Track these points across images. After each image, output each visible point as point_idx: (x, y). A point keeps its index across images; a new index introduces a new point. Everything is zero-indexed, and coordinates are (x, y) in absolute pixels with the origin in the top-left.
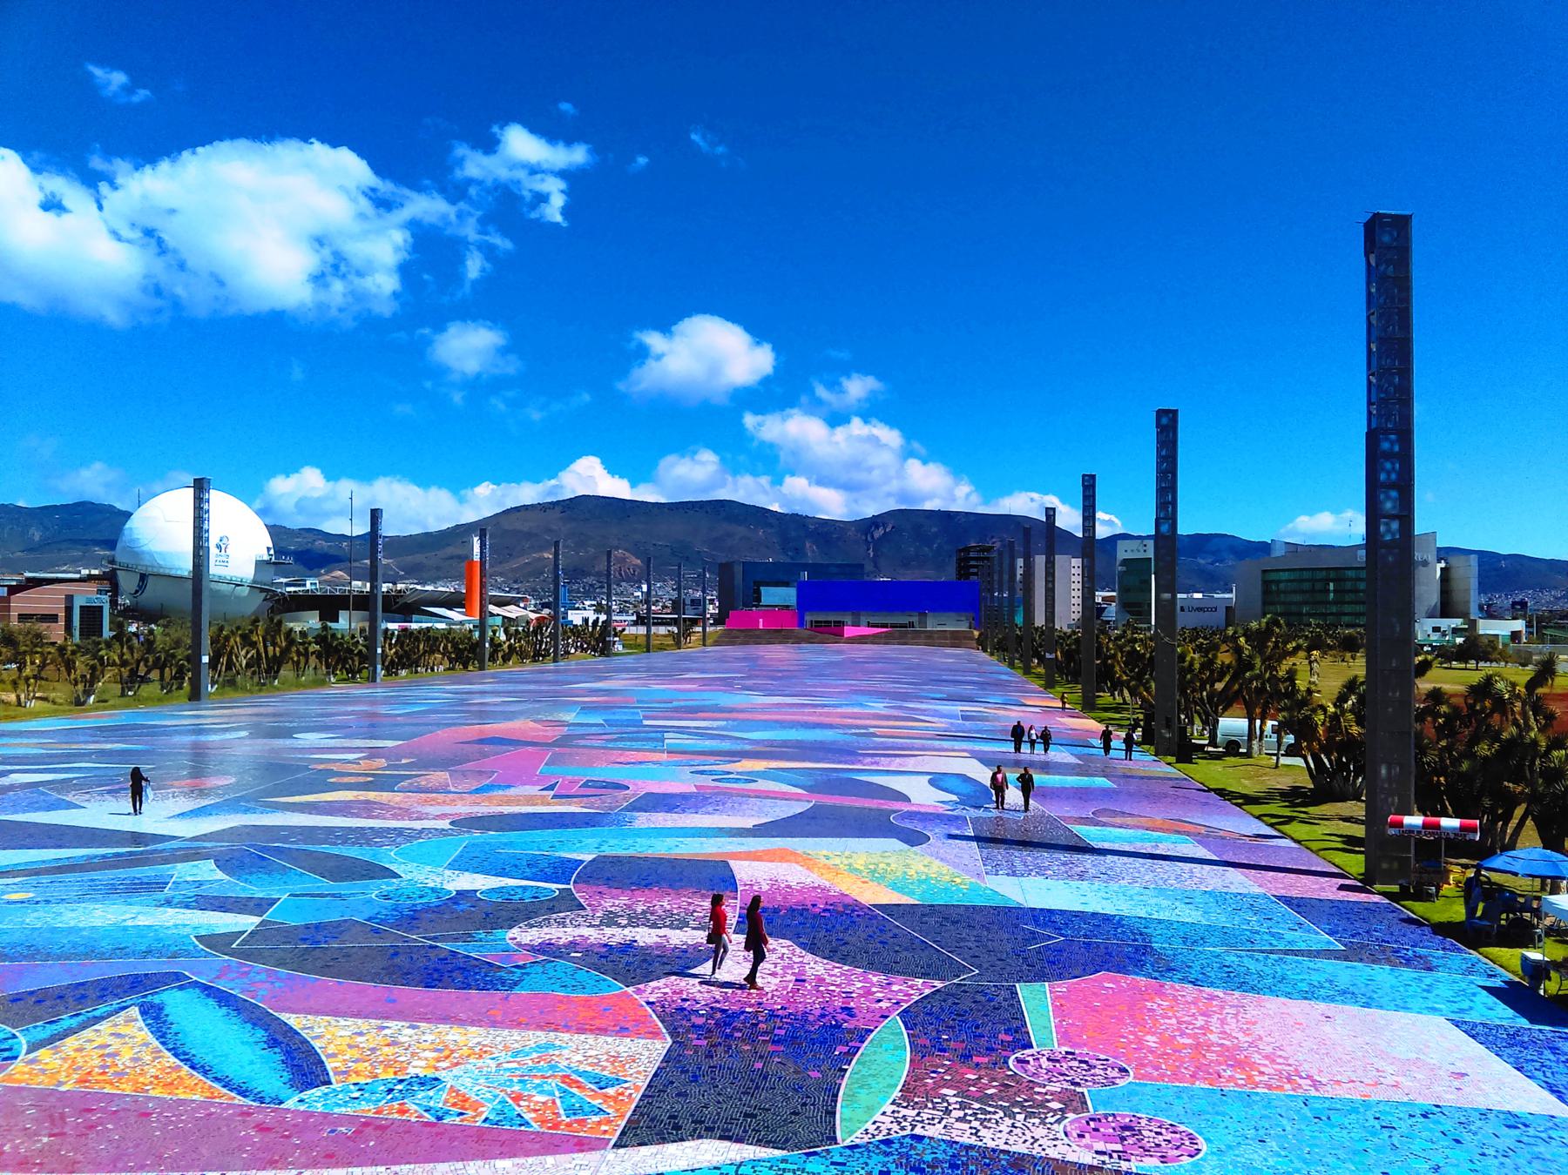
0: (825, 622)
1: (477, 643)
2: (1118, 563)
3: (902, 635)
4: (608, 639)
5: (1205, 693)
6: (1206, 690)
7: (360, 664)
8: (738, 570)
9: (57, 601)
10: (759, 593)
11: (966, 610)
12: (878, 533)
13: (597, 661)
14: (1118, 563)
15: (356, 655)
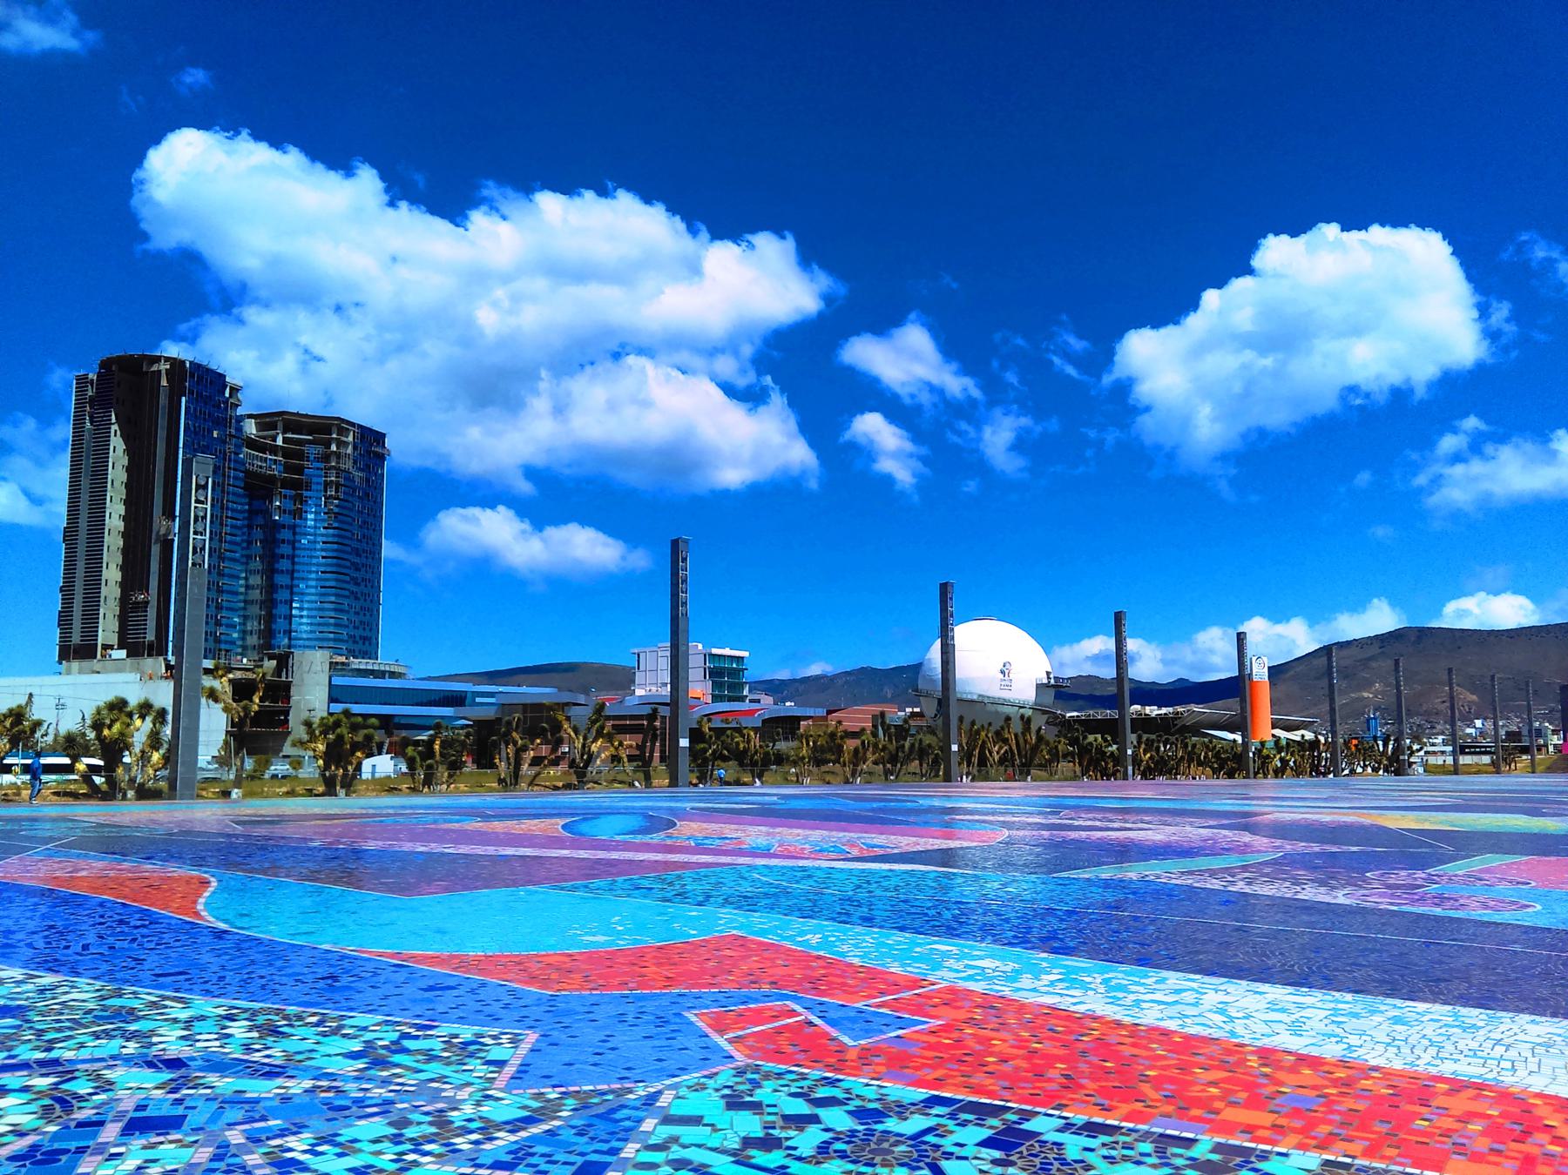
1: (1241, 754)
4: (1401, 757)
7: (1114, 767)
8: (99, 656)
15: (1109, 757)
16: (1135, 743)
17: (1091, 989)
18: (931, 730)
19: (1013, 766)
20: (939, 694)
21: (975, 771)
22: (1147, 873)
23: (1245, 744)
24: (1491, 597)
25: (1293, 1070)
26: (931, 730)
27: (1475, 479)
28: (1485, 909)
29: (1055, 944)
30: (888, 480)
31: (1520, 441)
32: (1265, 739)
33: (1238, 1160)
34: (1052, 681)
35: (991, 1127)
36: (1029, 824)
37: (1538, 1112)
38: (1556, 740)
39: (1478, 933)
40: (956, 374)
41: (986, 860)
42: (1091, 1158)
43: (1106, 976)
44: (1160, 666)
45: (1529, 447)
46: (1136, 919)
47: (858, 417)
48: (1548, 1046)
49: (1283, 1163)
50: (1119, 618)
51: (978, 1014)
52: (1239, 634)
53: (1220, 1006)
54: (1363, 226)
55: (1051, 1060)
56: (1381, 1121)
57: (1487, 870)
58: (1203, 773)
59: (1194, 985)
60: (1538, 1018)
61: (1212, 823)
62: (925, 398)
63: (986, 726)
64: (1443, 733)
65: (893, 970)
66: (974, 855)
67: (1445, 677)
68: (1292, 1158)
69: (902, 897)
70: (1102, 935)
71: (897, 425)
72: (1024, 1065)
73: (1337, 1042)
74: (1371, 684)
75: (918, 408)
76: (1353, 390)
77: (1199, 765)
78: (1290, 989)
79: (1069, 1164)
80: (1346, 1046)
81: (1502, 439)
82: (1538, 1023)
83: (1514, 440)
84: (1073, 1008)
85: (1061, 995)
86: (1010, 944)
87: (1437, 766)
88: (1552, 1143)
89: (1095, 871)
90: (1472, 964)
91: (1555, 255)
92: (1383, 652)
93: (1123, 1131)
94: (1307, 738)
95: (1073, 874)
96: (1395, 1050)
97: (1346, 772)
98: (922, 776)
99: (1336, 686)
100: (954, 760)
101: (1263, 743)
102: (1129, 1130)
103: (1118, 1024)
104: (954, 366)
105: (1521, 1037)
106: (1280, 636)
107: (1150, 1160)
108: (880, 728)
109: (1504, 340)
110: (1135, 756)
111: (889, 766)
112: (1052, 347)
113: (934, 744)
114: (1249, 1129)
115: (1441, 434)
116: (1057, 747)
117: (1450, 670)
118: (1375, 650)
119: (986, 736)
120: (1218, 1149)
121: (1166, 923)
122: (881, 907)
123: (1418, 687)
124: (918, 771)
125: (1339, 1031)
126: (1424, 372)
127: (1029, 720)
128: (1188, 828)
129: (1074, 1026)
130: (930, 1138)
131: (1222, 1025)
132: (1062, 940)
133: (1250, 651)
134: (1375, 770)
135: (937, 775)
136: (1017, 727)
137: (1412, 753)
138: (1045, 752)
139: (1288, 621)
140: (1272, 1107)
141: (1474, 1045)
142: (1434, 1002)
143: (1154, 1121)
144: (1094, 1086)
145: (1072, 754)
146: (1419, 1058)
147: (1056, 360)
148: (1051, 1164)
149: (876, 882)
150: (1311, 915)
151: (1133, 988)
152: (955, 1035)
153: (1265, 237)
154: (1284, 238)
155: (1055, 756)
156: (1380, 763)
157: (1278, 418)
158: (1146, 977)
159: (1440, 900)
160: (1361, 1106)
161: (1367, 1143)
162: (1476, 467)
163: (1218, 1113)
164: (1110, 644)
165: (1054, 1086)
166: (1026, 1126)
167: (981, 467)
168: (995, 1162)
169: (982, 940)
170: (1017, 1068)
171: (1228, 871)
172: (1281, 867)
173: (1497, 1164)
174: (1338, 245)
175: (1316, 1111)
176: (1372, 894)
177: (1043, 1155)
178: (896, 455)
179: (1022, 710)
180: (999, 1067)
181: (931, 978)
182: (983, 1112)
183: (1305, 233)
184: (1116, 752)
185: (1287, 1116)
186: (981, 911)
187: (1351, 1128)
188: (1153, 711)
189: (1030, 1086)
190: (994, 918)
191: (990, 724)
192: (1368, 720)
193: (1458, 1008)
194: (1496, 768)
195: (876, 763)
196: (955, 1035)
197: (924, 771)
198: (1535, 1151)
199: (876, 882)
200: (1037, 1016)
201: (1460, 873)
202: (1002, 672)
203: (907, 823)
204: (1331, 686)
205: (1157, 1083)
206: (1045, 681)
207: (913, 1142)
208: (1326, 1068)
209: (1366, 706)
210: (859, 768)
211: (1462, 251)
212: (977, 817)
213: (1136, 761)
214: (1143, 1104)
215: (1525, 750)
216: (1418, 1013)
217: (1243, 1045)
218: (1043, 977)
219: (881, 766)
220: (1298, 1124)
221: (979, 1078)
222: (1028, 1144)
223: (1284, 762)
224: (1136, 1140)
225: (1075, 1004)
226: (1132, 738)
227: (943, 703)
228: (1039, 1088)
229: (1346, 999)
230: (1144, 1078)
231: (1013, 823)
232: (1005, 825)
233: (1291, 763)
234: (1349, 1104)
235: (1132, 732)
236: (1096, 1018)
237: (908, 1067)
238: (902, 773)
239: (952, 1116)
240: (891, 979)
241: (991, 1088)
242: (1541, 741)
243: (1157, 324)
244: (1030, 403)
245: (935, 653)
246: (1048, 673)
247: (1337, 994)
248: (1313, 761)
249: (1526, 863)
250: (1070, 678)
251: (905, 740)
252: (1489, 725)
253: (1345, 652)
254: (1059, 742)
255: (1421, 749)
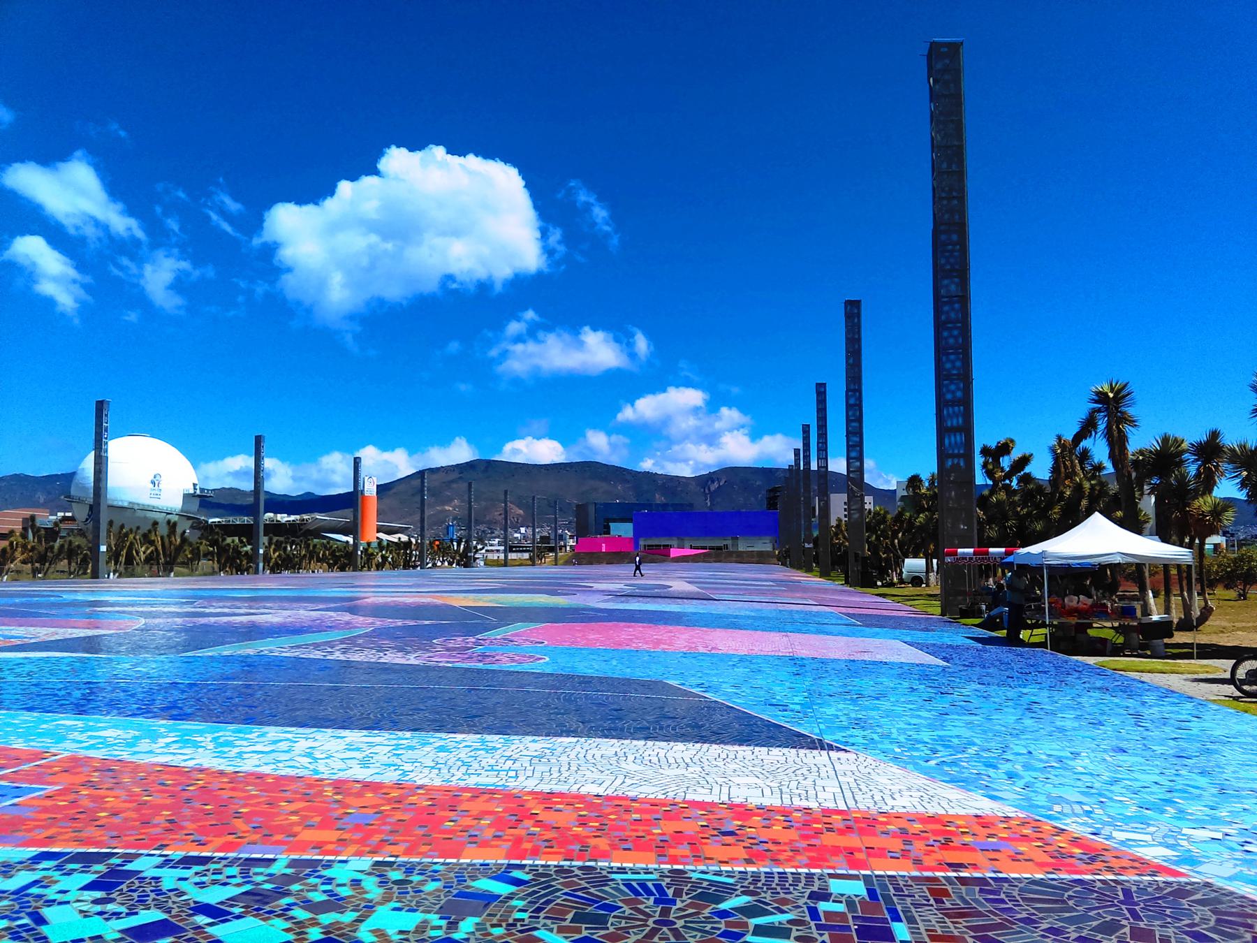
0: (656, 546)
1: (352, 553)
2: (897, 499)
3: (718, 555)
4: (469, 554)
5: (896, 541)
6: (897, 538)
7: (247, 563)
8: (592, 509)
9: (15, 523)
10: (608, 528)
11: (766, 534)
12: (714, 486)
13: (463, 571)
14: (897, 499)
15: (243, 556)
16: (267, 544)
17: (201, 747)
18: (81, 533)
19: (158, 564)
20: (91, 501)
21: (122, 569)
22: (262, 649)
23: (356, 545)
24: (535, 441)
25: (359, 795)
26: (81, 533)
27: (531, 355)
28: (512, 662)
29: (175, 712)
30: (50, 302)
31: (562, 331)
32: (371, 540)
33: (307, 871)
34: (198, 492)
35: (96, 872)
36: (165, 613)
37: (528, 805)
38: (571, 542)
39: (505, 679)
40: (122, 213)
41: (121, 645)
42: (184, 886)
43: (217, 735)
44: (291, 482)
45: (567, 337)
46: (248, 686)
47: (18, 238)
48: (540, 757)
49: (343, 868)
50: (259, 441)
51: (95, 777)
52: (355, 459)
53: (308, 751)
54: (462, 154)
55: (159, 808)
56: (420, 826)
57: (516, 635)
58: (321, 568)
59: (289, 736)
60: (536, 738)
61: (321, 606)
62: (90, 231)
63: (134, 529)
64: (498, 537)
65: (14, 746)
66: (109, 641)
67: (502, 497)
68: (350, 863)
69: (34, 681)
70: (217, 702)
71: (60, 252)
72: (134, 815)
73: (395, 770)
74: (451, 500)
75: (83, 240)
76: (450, 278)
77: (318, 561)
78: (365, 732)
79: (165, 894)
80: (401, 772)
81: (549, 329)
82: (536, 742)
83: (557, 330)
84: (183, 764)
85: (174, 754)
86: (134, 715)
87: (494, 561)
88: (535, 826)
89: (218, 649)
90: (499, 703)
91: (592, 200)
92: (461, 478)
93: (215, 860)
94: (402, 540)
95: (199, 653)
96: (437, 771)
97: (430, 565)
98: (71, 573)
99: (426, 502)
100: (103, 560)
101: (369, 544)
102: (221, 858)
103: (222, 773)
104: (120, 206)
105: (525, 752)
106: (386, 462)
107: (233, 881)
108: (30, 531)
109: (557, 256)
110: (266, 556)
111: (37, 565)
112: (209, 204)
113: (83, 546)
114: (319, 846)
115: (509, 321)
116: (198, 548)
117: (506, 492)
118: (455, 475)
119: (134, 538)
120: (293, 864)
121: (273, 687)
122: (12, 691)
123: (483, 503)
124: (66, 569)
125: (398, 762)
126: (503, 272)
127: (175, 524)
128: (302, 612)
129: (183, 779)
130: (35, 890)
131: (309, 766)
132: (181, 708)
133: (363, 472)
134: (450, 564)
135: (85, 573)
136: (163, 530)
137: (477, 551)
138: (187, 552)
139: (393, 450)
140: (339, 825)
141: (492, 762)
142: (469, 732)
143: (241, 848)
144: (194, 826)
145: (212, 553)
146: (453, 775)
147: (214, 217)
148: (148, 896)
149: (9, 670)
150: (389, 674)
151: (238, 743)
152: (72, 797)
153: (389, 148)
154: (404, 151)
155: (197, 555)
156: (454, 558)
157: (394, 292)
158: (251, 733)
159: (482, 658)
160: (407, 816)
161: (407, 844)
162: (531, 347)
163: (295, 836)
164: (250, 462)
165: (159, 830)
166: (129, 867)
167: (142, 301)
168: (96, 902)
169: (108, 713)
170: (126, 819)
171: (331, 644)
172: (376, 638)
173: (497, 846)
174: (443, 165)
175: (372, 825)
176: (438, 656)
177: (142, 889)
178: (56, 279)
179: (169, 516)
180: (109, 820)
181: (53, 750)
182: (87, 860)
183: (420, 150)
184: (250, 552)
185: (350, 831)
186: (110, 688)
187: (397, 834)
188: (283, 518)
189: (136, 832)
190: (122, 694)
191: (138, 528)
192: (448, 526)
193: (485, 736)
194: (532, 561)
195: (24, 562)
196: (72, 797)
197: (72, 569)
198: (523, 833)
199: (9, 670)
200: (149, 774)
201: (498, 637)
202: (153, 483)
203: (47, 615)
204: (423, 500)
205: (247, 817)
206: (192, 491)
207: (15, 897)
208: (384, 791)
209: (448, 516)
210: (7, 567)
211: (531, 186)
212: (117, 609)
213: (267, 558)
214: (234, 836)
215: (552, 549)
216: (456, 742)
217: (322, 780)
218: (160, 740)
219: (30, 565)
220: (358, 836)
221: (91, 832)
222: (128, 882)
223: (384, 558)
224: (225, 866)
225: (185, 760)
226: (264, 540)
227: (94, 509)
228: (144, 833)
229: (406, 736)
230: (237, 815)
231: (150, 612)
232: (142, 614)
233: (390, 559)
234: (399, 816)
235: (264, 535)
236: (202, 771)
237: (20, 831)
238: (51, 570)
239: (59, 868)
240: (13, 754)
241: (98, 839)
242: (562, 543)
243: (300, 201)
244: (190, 250)
245: (88, 465)
246: (195, 485)
247: (400, 733)
248: (406, 557)
249: (543, 628)
250: (214, 490)
251: (55, 541)
252: (530, 531)
253: (435, 477)
254: (201, 543)
255: (483, 548)
